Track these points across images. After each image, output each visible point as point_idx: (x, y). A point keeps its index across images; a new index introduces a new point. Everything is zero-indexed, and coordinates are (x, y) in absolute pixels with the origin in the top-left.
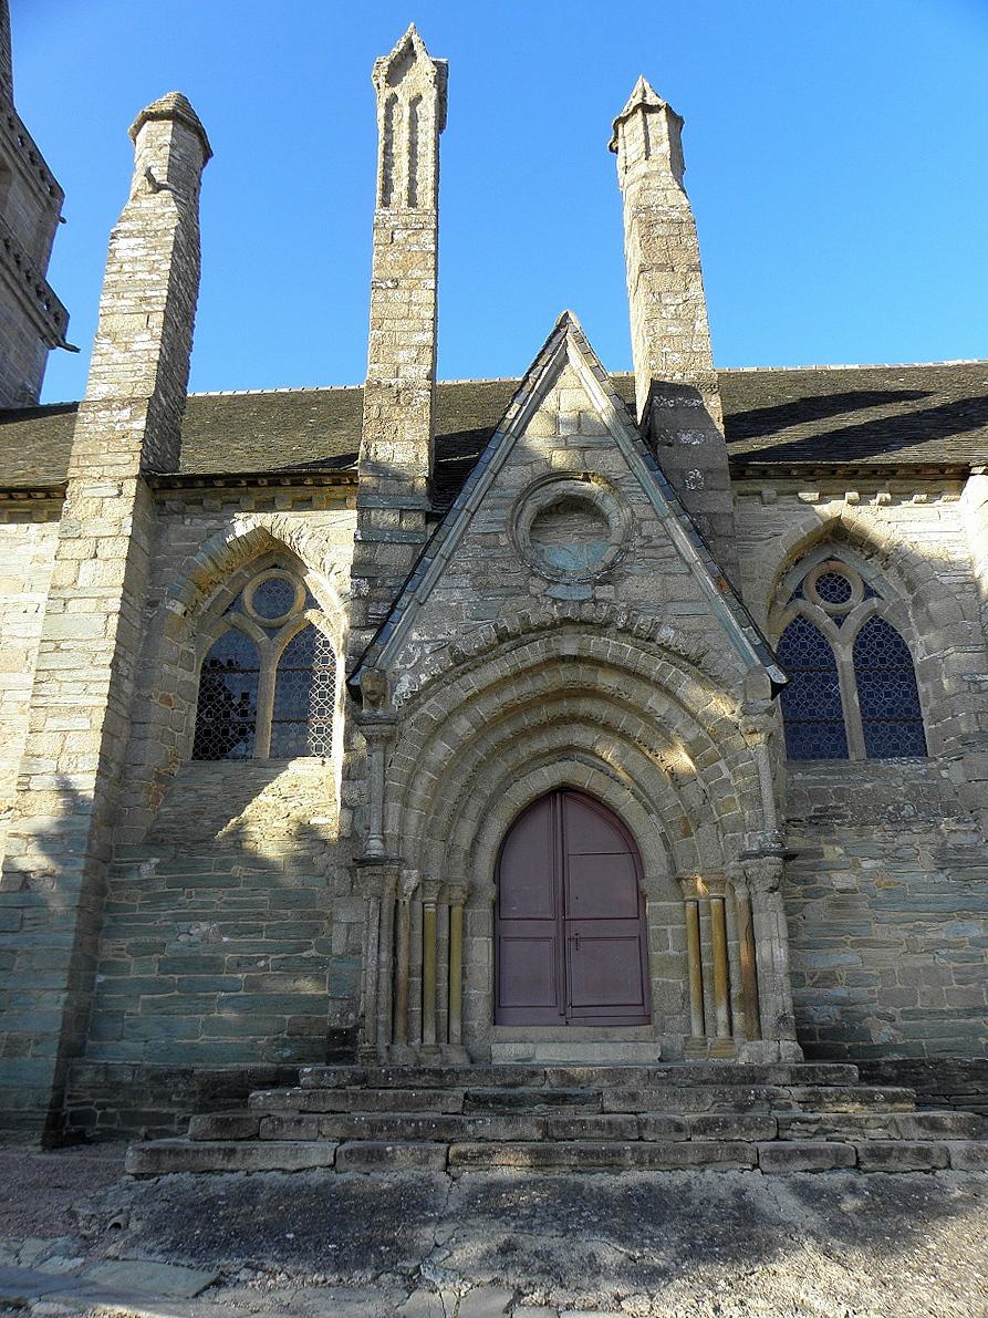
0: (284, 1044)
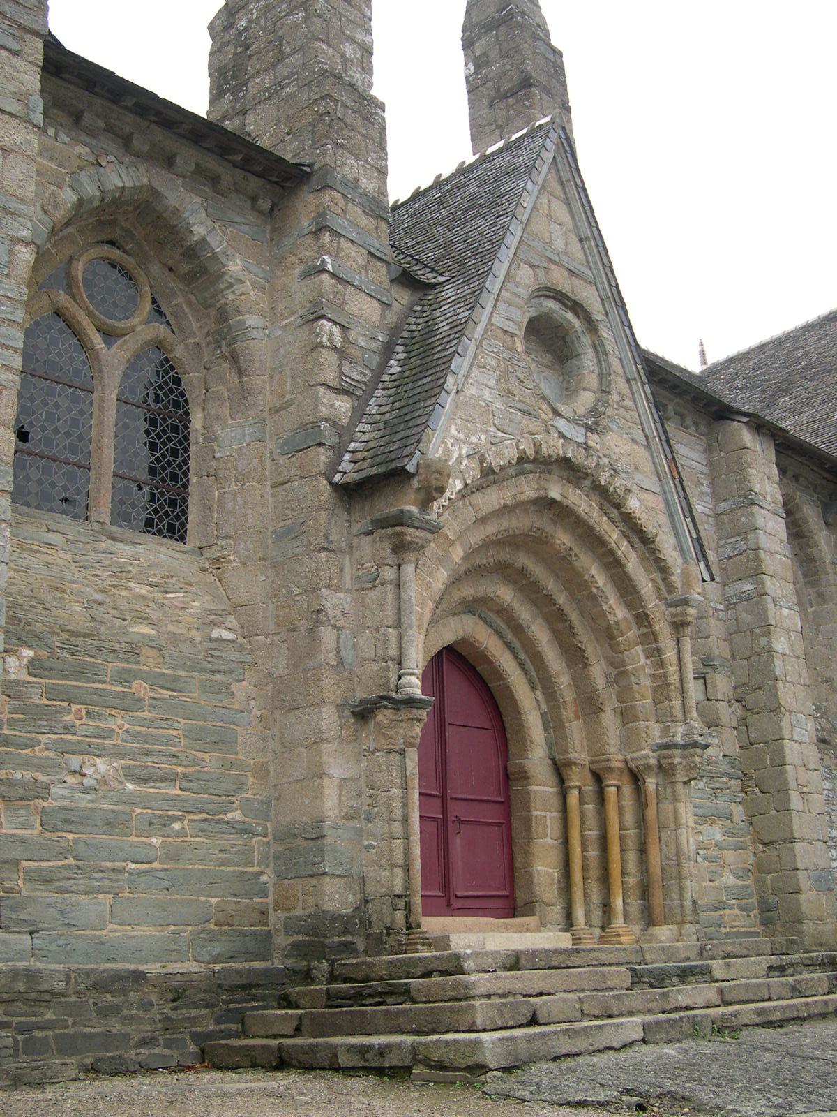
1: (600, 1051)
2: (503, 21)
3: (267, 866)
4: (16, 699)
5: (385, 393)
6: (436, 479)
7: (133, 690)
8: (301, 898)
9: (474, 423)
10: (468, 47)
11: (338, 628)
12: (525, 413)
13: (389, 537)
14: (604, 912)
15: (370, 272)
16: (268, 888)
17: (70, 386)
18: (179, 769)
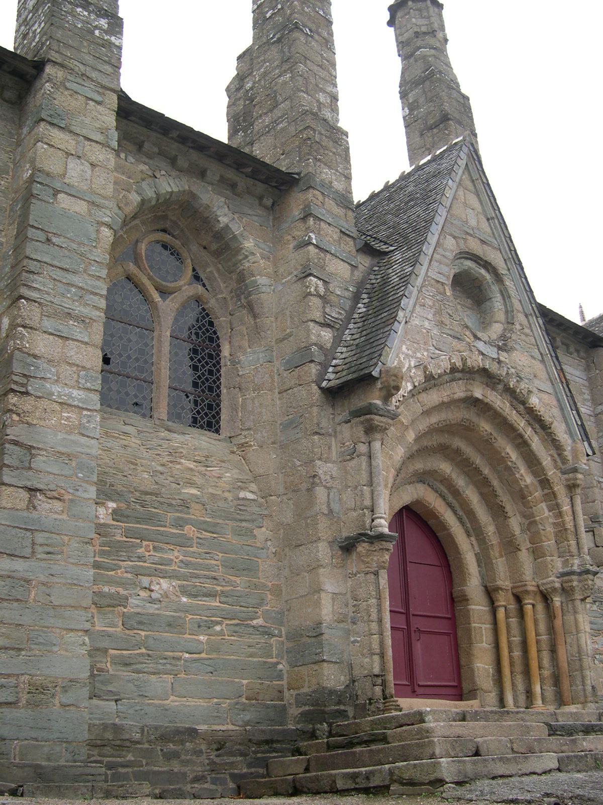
1: (526, 775)
2: (427, 78)
3: (282, 658)
4: (105, 536)
5: (356, 326)
6: (393, 380)
7: (185, 532)
8: (307, 680)
9: (417, 344)
10: (404, 97)
11: (328, 488)
12: (454, 337)
13: (362, 423)
14: (528, 697)
15: (342, 245)
16: (283, 674)
17: (138, 327)
18: (219, 588)
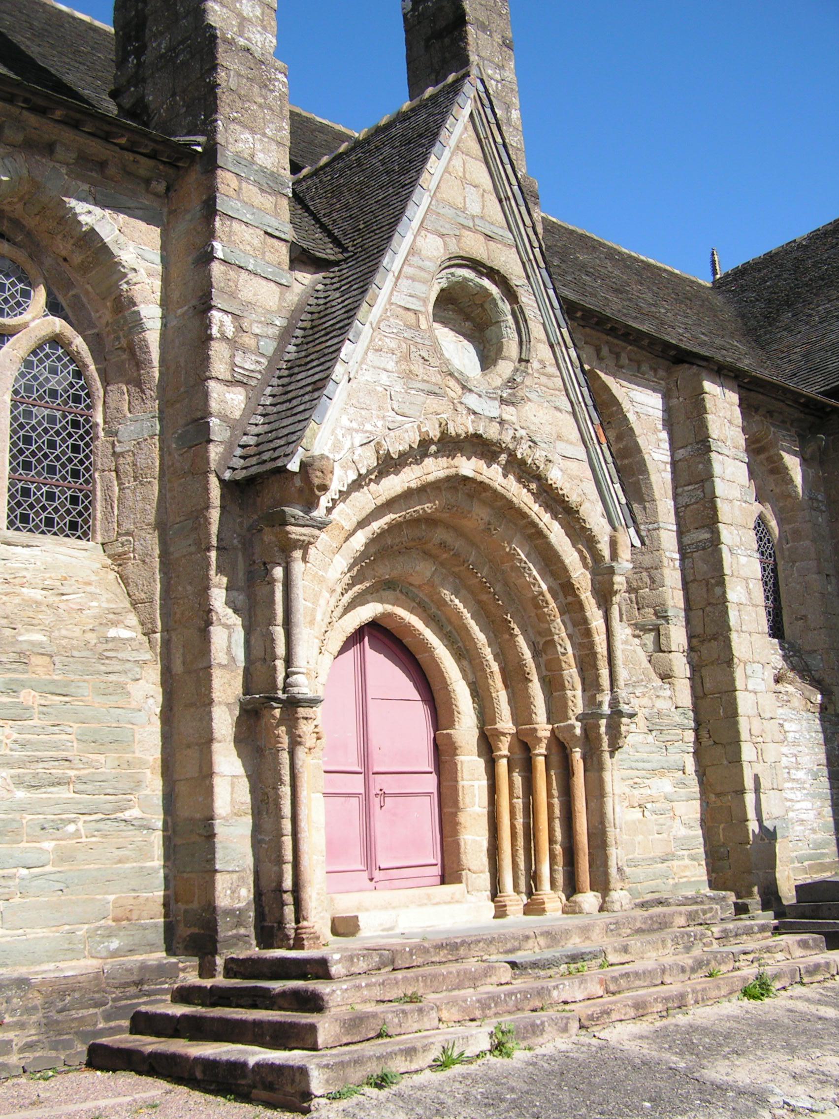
0: (110, 934)
18: (72, 773)
